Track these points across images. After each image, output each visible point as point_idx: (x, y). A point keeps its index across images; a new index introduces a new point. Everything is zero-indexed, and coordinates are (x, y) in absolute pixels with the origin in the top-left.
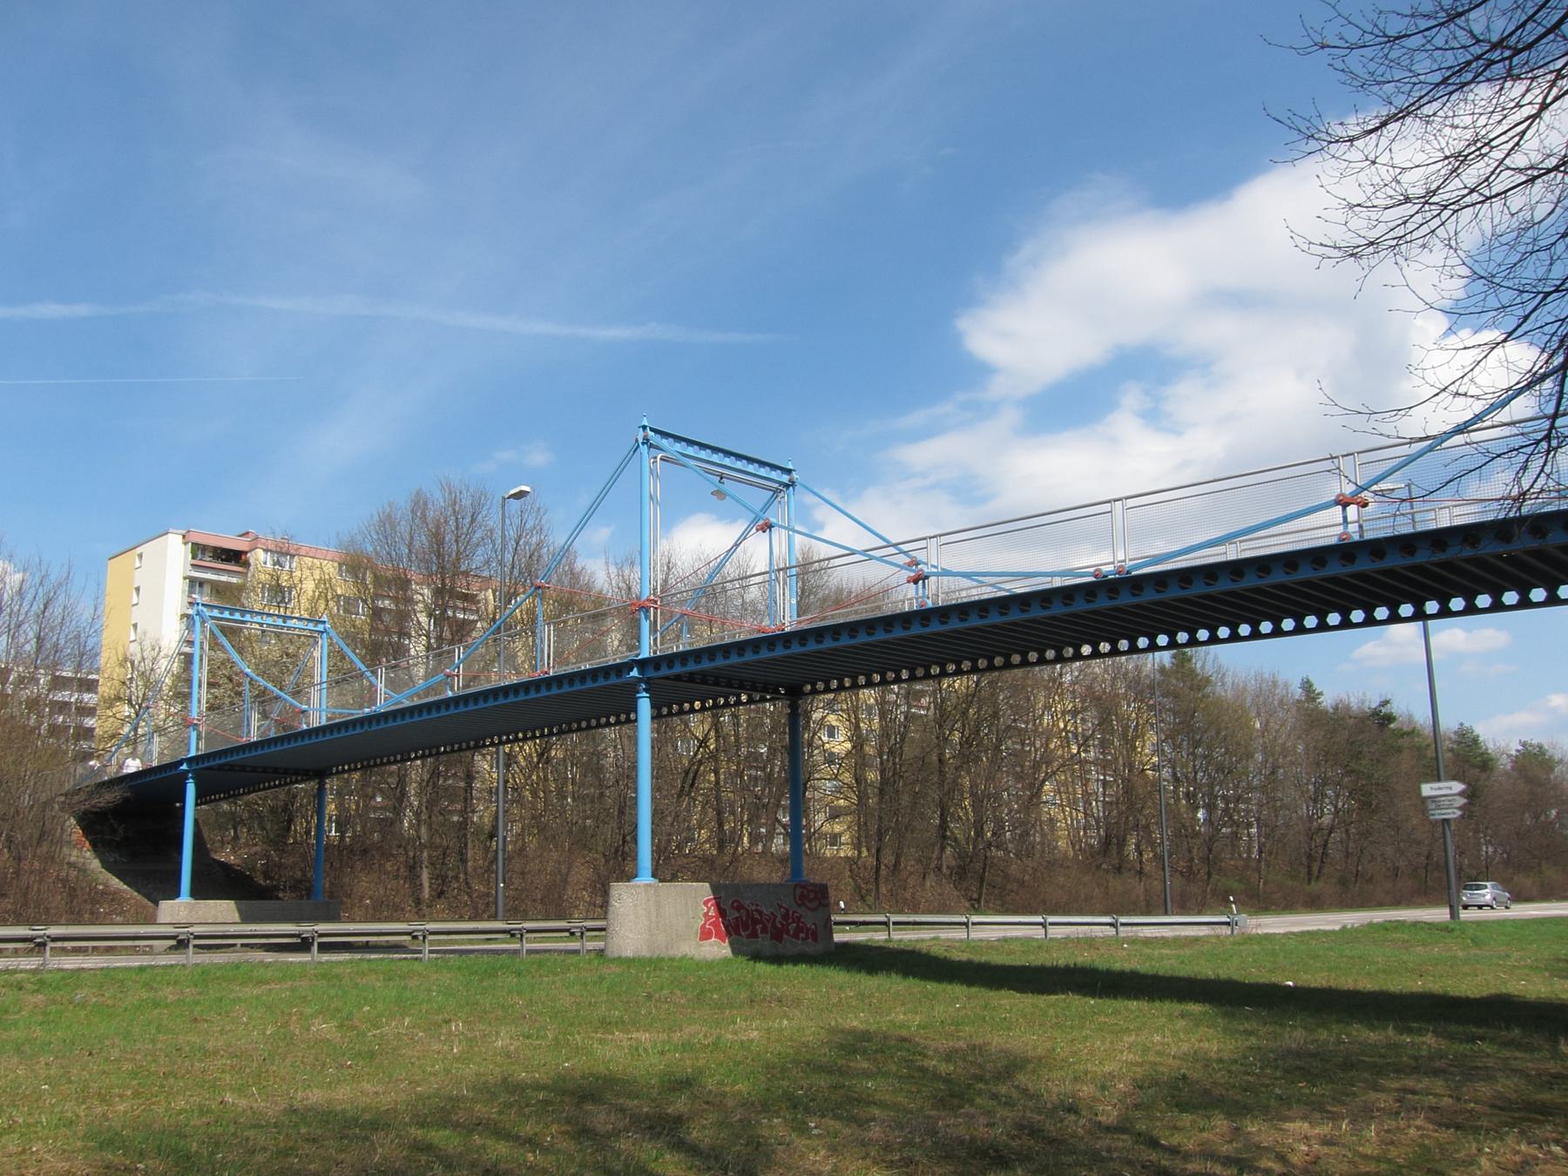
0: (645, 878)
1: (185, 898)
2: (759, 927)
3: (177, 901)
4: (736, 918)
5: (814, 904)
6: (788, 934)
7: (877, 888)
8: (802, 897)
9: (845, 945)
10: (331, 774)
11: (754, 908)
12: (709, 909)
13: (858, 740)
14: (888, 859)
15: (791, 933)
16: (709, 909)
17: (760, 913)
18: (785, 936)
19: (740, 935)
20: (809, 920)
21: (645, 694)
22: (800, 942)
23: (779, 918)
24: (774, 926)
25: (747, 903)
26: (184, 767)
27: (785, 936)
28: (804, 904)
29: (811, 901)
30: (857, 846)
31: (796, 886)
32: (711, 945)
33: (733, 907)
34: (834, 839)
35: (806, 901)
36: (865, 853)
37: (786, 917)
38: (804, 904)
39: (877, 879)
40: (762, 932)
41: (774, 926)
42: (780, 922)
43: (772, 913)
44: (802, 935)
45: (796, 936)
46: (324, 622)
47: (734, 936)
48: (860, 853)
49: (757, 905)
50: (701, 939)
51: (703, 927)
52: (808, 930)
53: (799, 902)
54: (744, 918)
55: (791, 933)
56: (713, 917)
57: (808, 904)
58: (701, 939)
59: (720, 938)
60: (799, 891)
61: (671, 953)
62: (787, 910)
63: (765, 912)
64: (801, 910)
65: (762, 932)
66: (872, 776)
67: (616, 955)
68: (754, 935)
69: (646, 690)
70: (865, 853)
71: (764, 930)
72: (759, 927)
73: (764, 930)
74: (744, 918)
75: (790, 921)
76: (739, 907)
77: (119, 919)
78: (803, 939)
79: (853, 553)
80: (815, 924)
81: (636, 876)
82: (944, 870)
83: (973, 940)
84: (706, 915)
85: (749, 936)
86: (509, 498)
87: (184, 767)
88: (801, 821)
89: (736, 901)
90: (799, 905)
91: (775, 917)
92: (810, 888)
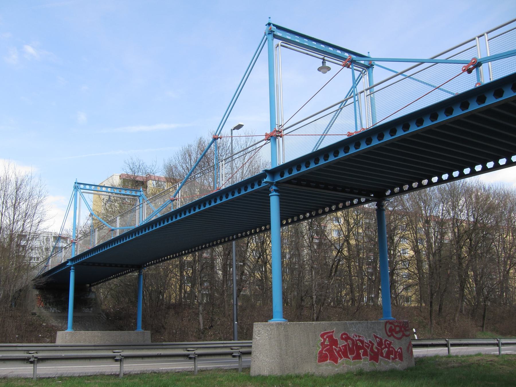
0: (278, 319)
1: (69, 330)
2: (361, 351)
3: (66, 331)
4: (345, 346)
5: (399, 335)
6: (382, 356)
7: (431, 322)
8: (391, 330)
9: (421, 361)
10: (144, 267)
11: (357, 338)
12: (325, 340)
13: (417, 251)
14: (436, 307)
15: (384, 355)
16: (325, 340)
17: (362, 342)
18: (380, 357)
19: (349, 358)
20: (397, 345)
21: (274, 193)
22: (391, 361)
23: (375, 345)
24: (372, 350)
25: (352, 335)
26: (69, 264)
27: (380, 357)
28: (392, 335)
29: (396, 333)
30: (419, 301)
31: (386, 323)
32: (327, 365)
33: (342, 338)
34: (407, 299)
35: (394, 333)
36: (424, 305)
37: (380, 344)
38: (392, 335)
39: (431, 316)
40: (363, 355)
41: (372, 350)
42: (376, 348)
43: (370, 342)
44: (392, 356)
45: (388, 357)
46: (141, 191)
47: (344, 358)
48: (421, 304)
49: (359, 336)
50: (319, 361)
51: (321, 352)
52: (396, 352)
53: (389, 334)
54: (351, 346)
55: (384, 355)
56: (327, 345)
57: (395, 335)
58: (319, 361)
59: (333, 360)
60: (388, 326)
61: (297, 372)
62: (381, 340)
63: (365, 341)
64: (391, 339)
65: (363, 355)
66: (426, 267)
67: (257, 373)
68: (358, 357)
69: (275, 191)
70: (424, 305)
71: (365, 354)
72: (361, 351)
73: (365, 354)
74: (351, 346)
75: (383, 346)
76: (347, 338)
77: (48, 340)
78: (393, 359)
79: (422, 63)
80: (400, 348)
81: (272, 318)
82: (464, 312)
83: (503, 355)
84: (322, 344)
85: (354, 358)
86: (234, 129)
87: (69, 264)
88: (378, 240)
89: (344, 334)
90: (389, 336)
91: (373, 344)
92: (396, 324)
